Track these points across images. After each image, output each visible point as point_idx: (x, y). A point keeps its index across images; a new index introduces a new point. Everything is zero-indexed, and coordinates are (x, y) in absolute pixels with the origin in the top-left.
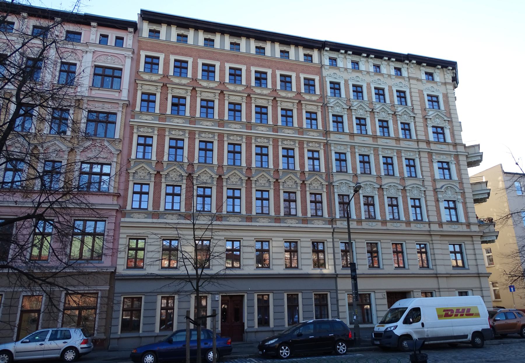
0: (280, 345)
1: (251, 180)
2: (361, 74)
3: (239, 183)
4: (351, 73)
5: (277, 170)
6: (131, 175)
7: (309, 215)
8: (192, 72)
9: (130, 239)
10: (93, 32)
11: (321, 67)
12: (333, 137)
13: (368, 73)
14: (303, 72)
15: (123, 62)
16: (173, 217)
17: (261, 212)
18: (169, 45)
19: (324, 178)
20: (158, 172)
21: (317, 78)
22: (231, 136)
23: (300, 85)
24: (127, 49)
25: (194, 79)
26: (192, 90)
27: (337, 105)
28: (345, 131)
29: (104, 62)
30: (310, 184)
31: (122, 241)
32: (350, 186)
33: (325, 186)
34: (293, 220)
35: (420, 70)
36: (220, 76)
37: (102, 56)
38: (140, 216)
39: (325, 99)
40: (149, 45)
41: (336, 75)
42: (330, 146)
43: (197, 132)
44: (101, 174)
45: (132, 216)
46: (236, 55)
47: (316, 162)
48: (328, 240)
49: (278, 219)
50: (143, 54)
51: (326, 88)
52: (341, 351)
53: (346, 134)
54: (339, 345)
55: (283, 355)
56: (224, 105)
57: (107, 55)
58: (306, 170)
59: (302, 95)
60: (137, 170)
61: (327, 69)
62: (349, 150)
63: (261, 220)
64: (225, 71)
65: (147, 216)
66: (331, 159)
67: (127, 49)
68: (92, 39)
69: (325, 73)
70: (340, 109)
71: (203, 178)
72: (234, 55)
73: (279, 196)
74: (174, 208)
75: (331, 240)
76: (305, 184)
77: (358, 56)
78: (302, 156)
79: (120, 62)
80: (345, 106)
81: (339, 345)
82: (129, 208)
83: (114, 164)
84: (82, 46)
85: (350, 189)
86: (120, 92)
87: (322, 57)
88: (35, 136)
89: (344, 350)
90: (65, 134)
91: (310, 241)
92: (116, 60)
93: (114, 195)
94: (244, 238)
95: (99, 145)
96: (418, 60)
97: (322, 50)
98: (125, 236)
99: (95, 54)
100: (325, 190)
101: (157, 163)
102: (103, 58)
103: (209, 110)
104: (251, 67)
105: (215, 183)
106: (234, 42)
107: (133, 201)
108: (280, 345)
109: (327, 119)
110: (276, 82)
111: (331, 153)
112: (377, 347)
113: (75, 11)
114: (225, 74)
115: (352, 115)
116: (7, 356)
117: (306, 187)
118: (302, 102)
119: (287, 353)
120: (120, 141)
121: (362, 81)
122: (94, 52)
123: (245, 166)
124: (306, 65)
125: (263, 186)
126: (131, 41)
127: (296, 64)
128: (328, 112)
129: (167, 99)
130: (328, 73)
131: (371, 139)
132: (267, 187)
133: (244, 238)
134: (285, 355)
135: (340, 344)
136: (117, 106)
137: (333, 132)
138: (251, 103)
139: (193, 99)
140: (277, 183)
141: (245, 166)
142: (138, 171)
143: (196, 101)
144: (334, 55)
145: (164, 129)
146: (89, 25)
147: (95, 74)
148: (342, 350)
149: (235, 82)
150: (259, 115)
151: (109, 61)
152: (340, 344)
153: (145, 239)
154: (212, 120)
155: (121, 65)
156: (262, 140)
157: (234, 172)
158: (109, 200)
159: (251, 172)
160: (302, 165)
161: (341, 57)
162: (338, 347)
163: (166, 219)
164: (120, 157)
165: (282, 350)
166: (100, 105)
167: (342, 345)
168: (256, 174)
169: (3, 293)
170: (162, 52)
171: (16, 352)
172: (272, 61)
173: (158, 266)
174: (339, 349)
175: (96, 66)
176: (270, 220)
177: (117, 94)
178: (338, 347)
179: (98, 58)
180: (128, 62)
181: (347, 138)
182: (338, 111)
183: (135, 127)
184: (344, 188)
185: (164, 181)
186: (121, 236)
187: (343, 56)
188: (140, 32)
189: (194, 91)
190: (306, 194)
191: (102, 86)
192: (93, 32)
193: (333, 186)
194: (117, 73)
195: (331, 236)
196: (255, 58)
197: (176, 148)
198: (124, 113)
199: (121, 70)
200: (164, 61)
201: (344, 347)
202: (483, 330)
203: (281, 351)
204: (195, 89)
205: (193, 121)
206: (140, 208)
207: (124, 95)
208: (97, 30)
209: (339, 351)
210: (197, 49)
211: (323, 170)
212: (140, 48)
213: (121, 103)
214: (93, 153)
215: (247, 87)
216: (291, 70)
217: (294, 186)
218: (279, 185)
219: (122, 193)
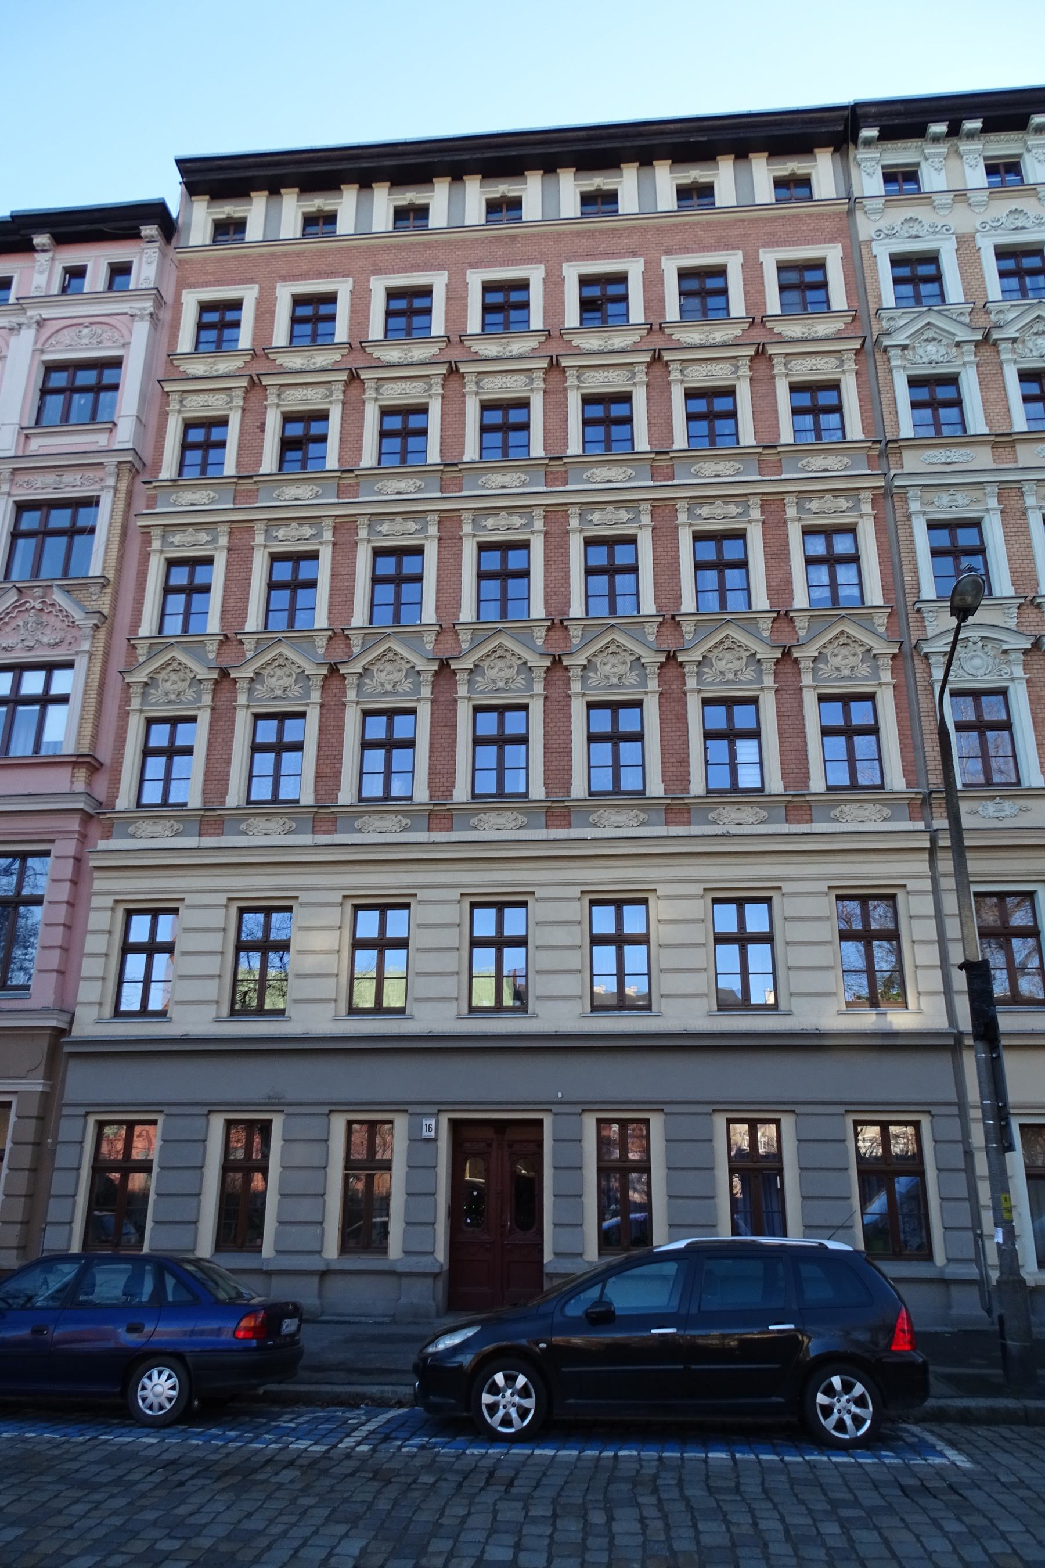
0: (486, 1365)
1: (566, 669)
2: (1033, 201)
3: (519, 683)
4: (881, 212)
5: (673, 617)
6: (136, 690)
7: (697, 787)
8: (351, 324)
9: (474, 905)
10: (150, 257)
11: (851, 212)
12: (912, 461)
13: (961, 195)
14: (773, 242)
15: (125, 332)
16: (866, 813)
17: (846, 782)
18: (273, 255)
19: (881, 630)
20: (671, 657)
21: (833, 256)
23: (762, 292)
25: (757, 321)
26: (446, 378)
27: (929, 334)
28: (971, 431)
29: (70, 348)
30: (815, 659)
31: (98, 920)
32: (1005, 652)
33: (885, 662)
34: (747, 808)
35: (961, 157)
36: (447, 320)
37: (65, 331)
38: (159, 829)
39: (874, 322)
40: (209, 268)
41: (916, 225)
42: (906, 500)
43: (363, 521)
45: (357, 824)
46: (507, 237)
47: (845, 574)
48: (911, 885)
49: (681, 812)
51: (877, 281)
52: (841, 1426)
53: (977, 440)
54: (830, 1391)
55: (494, 1421)
56: (463, 414)
58: (797, 605)
59: (769, 325)
60: (262, 667)
61: (875, 212)
62: (993, 502)
63: (610, 816)
64: (466, 298)
65: (766, 814)
66: (913, 551)
68: (147, 279)
69: (865, 227)
70: (943, 351)
71: (721, 665)
72: (498, 239)
73: (683, 718)
74: (742, 785)
75: (927, 885)
76: (796, 661)
77: (1013, 135)
78: (777, 555)
79: (116, 335)
80: (963, 335)
81: (830, 1391)
82: (124, 801)
83: (81, 663)
85: (1008, 662)
86: (111, 430)
87: (854, 171)
89: (858, 1421)
92: (104, 335)
93: (75, 765)
94: (787, 887)
95: (38, 606)
96: (885, 122)
97: (851, 146)
98: (109, 901)
100: (886, 676)
101: (221, 643)
103: (718, 423)
104: (663, 258)
105: (426, 692)
106: (498, 195)
107: (251, 776)
108: (486, 1365)
109: (884, 398)
110: (662, 300)
111: (910, 527)
112: (393, 1413)
114: (466, 310)
115: (1001, 365)
117: (234, 691)
118: (771, 350)
119: (523, 1413)
120: (104, 583)
121: (935, 233)
122: (38, 323)
123: (766, 606)
124: (783, 217)
125: (850, 678)
126: (154, 267)
127: (742, 221)
128: (891, 371)
129: (262, 428)
130: (882, 224)
131: (987, 450)
132: (297, 698)
133: (787, 887)
134: (506, 1422)
135: (836, 1381)
136: (97, 474)
137: (916, 444)
138: (565, 389)
139: (659, 393)
140: (788, 668)
141: (766, 606)
142: (598, 660)
143: (363, 418)
144: (901, 154)
145: (248, 527)
146: (29, 248)
147: (45, 391)
148: (847, 1419)
149: (705, 315)
150: (927, 413)
152: (836, 1381)
153: (768, 900)
154: (843, 446)
156: (294, 533)
157: (839, 630)
158: (59, 780)
159: (567, 639)
160: (780, 588)
161: (934, 155)
162: (821, 1399)
164: (102, 635)
165: (495, 1390)
166: (50, 478)
167: (847, 1387)
169: (14, 1099)
172: (645, 230)
173: (705, 1000)
174: (827, 1411)
175: (50, 368)
176: (643, 816)
178: (821, 1399)
179: (52, 341)
180: (141, 330)
181: (983, 458)
182: (934, 358)
183: (156, 532)
184: (977, 662)
185: (579, 690)
186: (96, 901)
187: (943, 148)
188: (183, 236)
189: (454, 378)
190: (801, 701)
191: (65, 419)
193: (926, 656)
195: (925, 867)
196: (579, 234)
197: (505, 575)
198: (122, 495)
200: (257, 309)
201: (860, 1402)
203: (487, 1399)
204: (660, 358)
205: (350, 485)
206: (275, 800)
207: (125, 435)
208: (53, 259)
209: (829, 1424)
210: (368, 247)
211: (875, 596)
212: (182, 284)
213: (111, 460)
214: (22, 631)
215: (854, 317)
216: (723, 245)
217: (749, 674)
218: (683, 675)
219: (105, 755)
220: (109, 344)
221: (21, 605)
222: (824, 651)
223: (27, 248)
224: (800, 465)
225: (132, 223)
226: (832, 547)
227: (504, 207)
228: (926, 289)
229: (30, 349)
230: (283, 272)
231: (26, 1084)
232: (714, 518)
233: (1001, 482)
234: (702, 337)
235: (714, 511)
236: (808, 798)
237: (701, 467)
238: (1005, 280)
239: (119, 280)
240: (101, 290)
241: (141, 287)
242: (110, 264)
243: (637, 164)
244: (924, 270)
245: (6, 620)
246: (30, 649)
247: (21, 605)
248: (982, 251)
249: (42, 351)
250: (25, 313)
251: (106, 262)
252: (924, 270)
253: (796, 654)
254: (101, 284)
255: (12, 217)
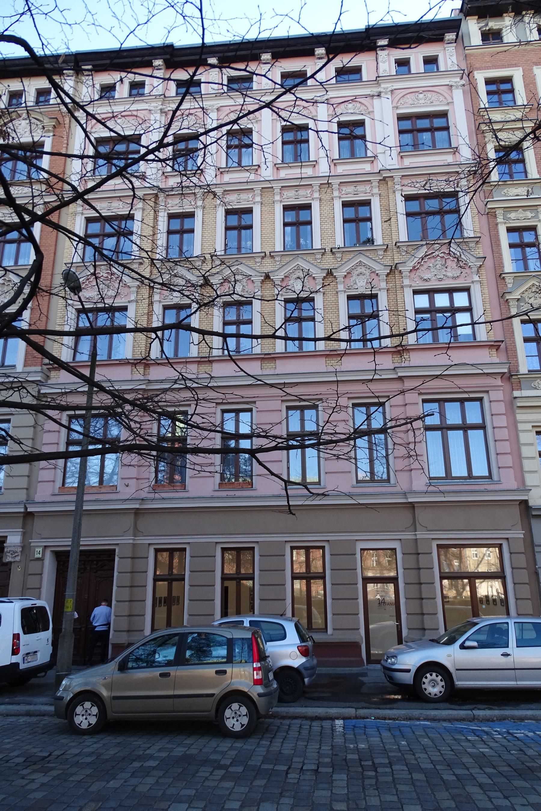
10: (451, 52)
22: (510, 212)
24: (448, 73)
29: (413, 105)
37: (408, 96)
44: (453, 310)
50: (480, 77)
57: (415, 91)
67: (448, 73)
79: (441, 98)
84: (121, 103)
88: (386, 250)
90: (373, 244)
91: (530, 431)
92: (433, 98)
98: (529, 426)
99: (394, 96)
102: (409, 99)
104: (535, 68)
113: (338, 29)
116: (428, 675)
120: (477, 240)
151: (420, 102)
155: (444, 105)
163: (536, 388)
168: (516, 286)
170: (516, 65)
171: (457, 670)
175: (401, 118)
177: (450, 159)
179: (401, 101)
180: (458, 96)
192: (451, 52)
194: (438, 122)
199: (444, 115)
202: (52, 645)
213: (316, 183)
220: (438, 103)
221: (429, 255)
222: (523, 295)
223: (373, 48)
224: (502, 193)
225: (150, 58)
226: (523, 238)
227: (490, 36)
228: (505, 97)
229: (391, 106)
230: (534, 60)
231: (514, 533)
232: (518, 219)
233: (505, 208)
234: (503, 116)
235: (517, 216)
236: (519, 376)
237: (507, 191)
238: (491, 96)
239: (42, 99)
240: (126, 97)
241: (449, 70)
242: (36, 89)
243: (477, 17)
244: (503, 87)
245: (422, 263)
246: (440, 280)
247: (429, 255)
248: (478, 80)
249: (397, 108)
250: (380, 85)
251: (34, 88)
252: (503, 87)
253: (508, 297)
254: (126, 94)
255: (366, 29)
